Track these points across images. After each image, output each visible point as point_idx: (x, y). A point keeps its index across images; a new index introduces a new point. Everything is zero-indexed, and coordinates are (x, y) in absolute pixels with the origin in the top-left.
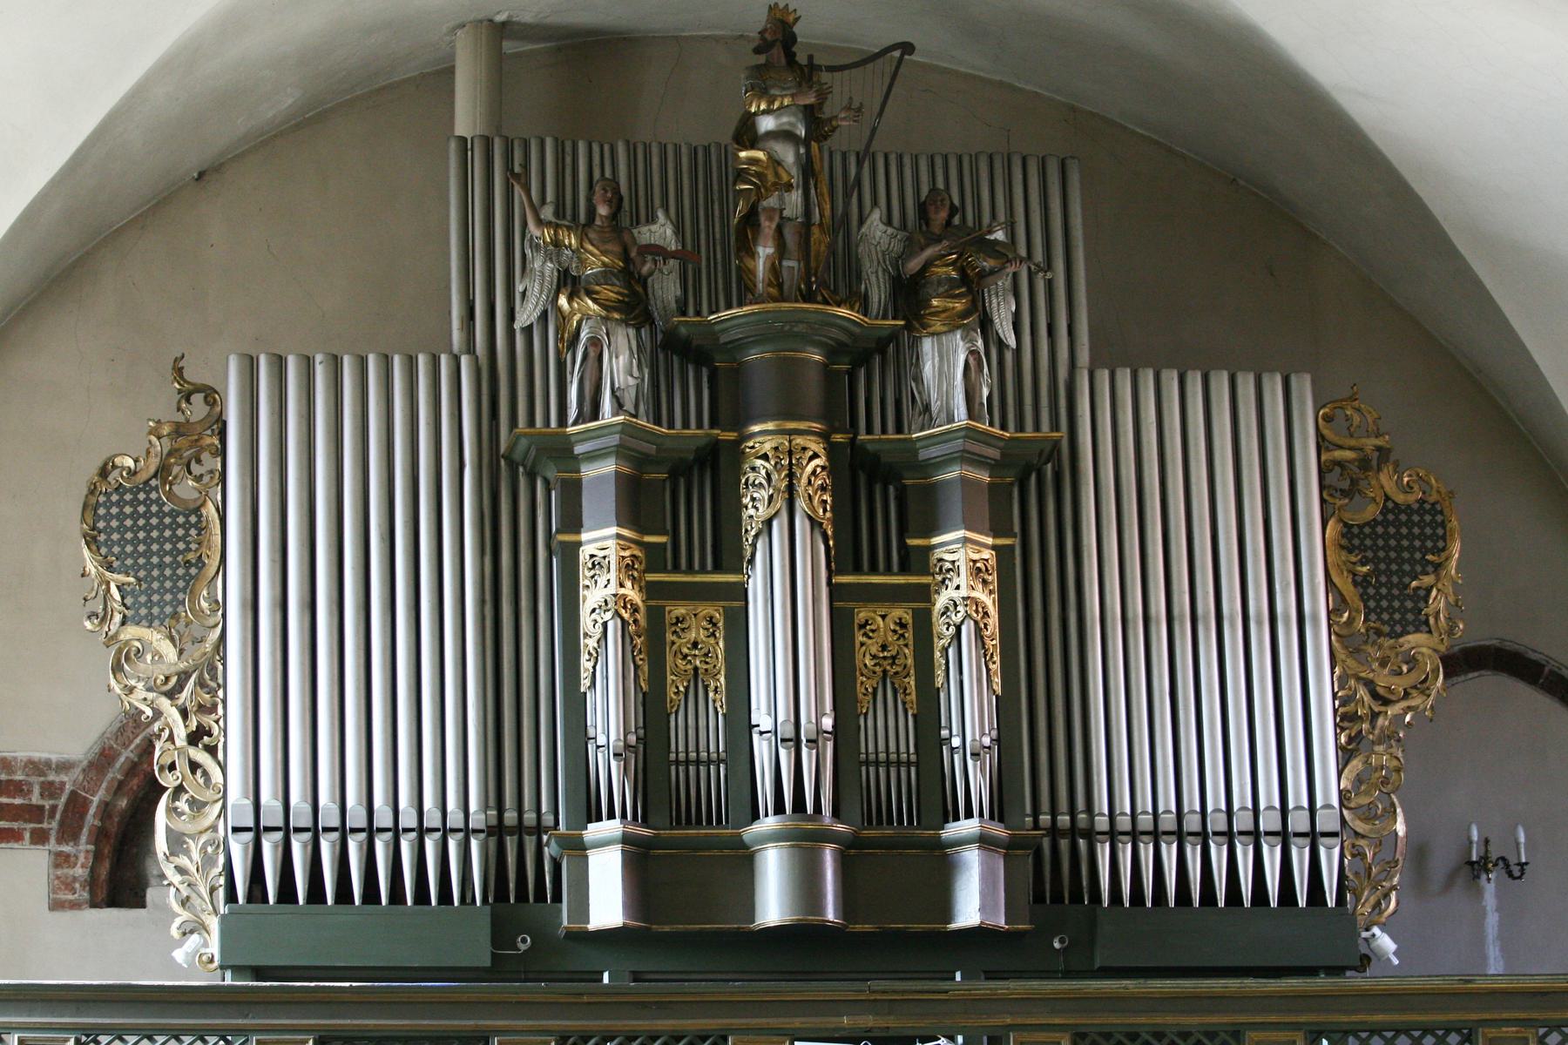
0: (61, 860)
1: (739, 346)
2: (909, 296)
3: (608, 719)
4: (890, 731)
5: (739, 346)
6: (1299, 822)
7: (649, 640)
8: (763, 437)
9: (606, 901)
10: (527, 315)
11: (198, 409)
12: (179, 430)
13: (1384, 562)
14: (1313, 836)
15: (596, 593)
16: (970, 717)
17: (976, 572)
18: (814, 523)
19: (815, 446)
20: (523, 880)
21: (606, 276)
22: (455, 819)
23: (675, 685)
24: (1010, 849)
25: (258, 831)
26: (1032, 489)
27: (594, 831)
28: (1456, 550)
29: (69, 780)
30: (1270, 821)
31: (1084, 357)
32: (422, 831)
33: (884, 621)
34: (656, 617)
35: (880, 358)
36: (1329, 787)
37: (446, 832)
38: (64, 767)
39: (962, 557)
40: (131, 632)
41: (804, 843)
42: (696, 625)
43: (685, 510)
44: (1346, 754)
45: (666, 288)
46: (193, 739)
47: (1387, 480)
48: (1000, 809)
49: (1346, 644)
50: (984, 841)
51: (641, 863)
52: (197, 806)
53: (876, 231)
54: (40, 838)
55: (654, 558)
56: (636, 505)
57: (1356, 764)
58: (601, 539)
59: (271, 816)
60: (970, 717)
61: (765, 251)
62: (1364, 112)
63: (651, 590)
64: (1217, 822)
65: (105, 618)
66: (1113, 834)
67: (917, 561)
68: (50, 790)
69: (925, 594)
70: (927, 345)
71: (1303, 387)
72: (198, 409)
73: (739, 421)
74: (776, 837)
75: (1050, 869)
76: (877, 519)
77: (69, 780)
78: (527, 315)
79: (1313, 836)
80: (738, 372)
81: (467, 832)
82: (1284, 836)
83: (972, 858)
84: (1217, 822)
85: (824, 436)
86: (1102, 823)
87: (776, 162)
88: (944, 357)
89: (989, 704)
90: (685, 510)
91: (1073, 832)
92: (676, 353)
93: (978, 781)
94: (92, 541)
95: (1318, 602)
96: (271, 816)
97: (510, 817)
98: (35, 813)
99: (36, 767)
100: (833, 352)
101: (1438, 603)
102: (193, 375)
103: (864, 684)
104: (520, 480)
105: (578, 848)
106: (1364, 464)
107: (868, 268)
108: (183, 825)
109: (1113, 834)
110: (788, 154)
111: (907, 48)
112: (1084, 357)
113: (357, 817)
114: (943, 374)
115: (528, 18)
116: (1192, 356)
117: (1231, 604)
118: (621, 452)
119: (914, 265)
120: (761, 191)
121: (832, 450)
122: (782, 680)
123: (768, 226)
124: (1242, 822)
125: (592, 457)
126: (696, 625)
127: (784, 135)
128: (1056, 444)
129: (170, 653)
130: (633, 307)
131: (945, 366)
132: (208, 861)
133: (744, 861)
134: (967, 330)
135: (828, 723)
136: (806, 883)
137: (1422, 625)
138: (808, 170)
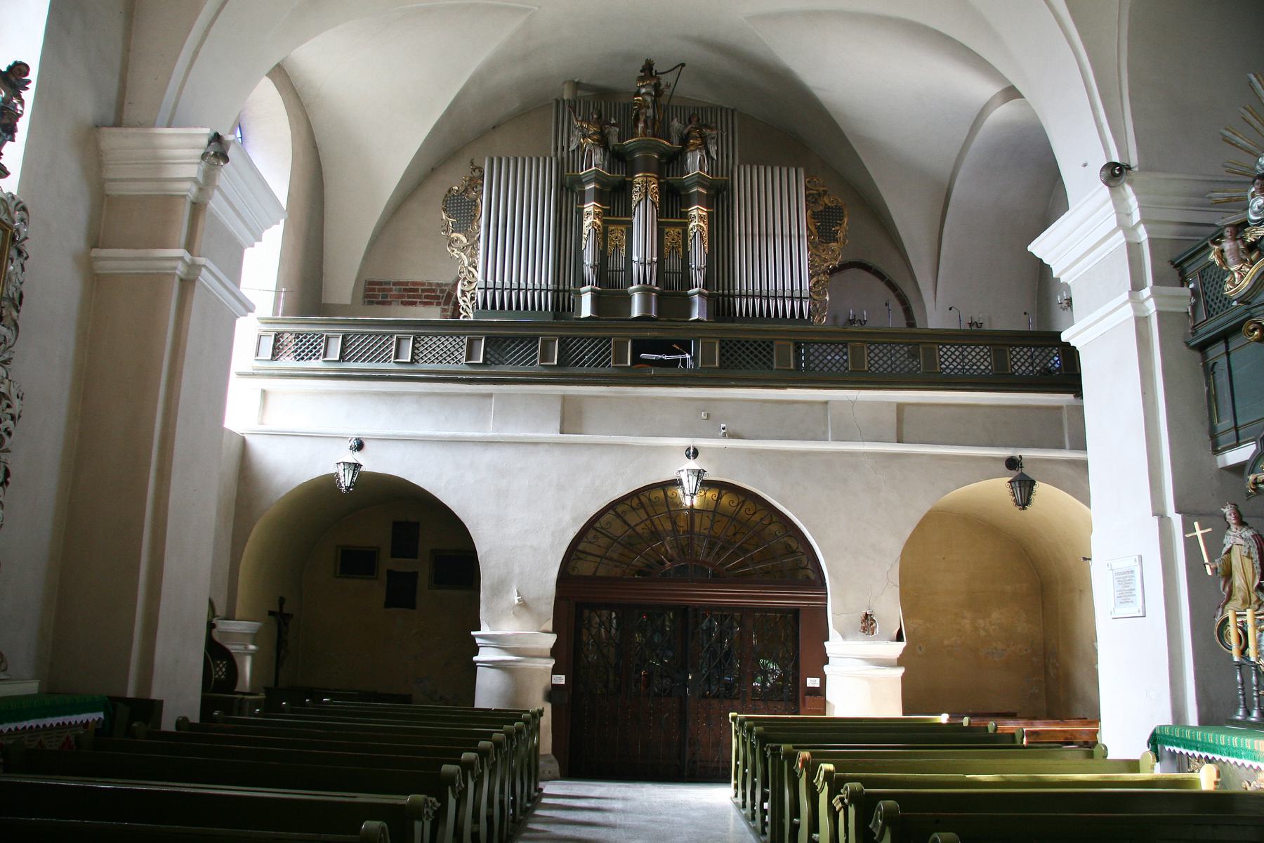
0: (444, 310)
1: (632, 153)
2: (684, 140)
3: (589, 258)
4: (674, 264)
5: (632, 153)
6: (797, 294)
7: (603, 235)
8: (639, 178)
9: (586, 311)
10: (573, 147)
11: (477, 173)
12: (471, 179)
13: (824, 225)
14: (801, 298)
15: (587, 222)
16: (698, 258)
17: (701, 217)
18: (653, 203)
19: (654, 180)
20: (563, 304)
21: (595, 133)
22: (544, 287)
23: (610, 249)
24: (709, 297)
25: (486, 289)
26: (719, 197)
27: (583, 289)
28: (846, 220)
29: (447, 289)
30: (788, 293)
31: (737, 162)
32: (534, 290)
33: (673, 232)
34: (605, 229)
35: (674, 160)
36: (806, 285)
37: (541, 290)
38: (447, 285)
39: (697, 212)
40: (454, 235)
41: (646, 291)
42: (617, 233)
43: (615, 199)
44: (811, 277)
45: (614, 140)
46: (470, 265)
47: (826, 200)
48: (705, 286)
49: (811, 244)
50: (700, 293)
51: (597, 300)
52: (470, 283)
53: (676, 124)
54: (438, 304)
55: (606, 213)
56: (599, 196)
57: (815, 279)
58: (589, 207)
59: (490, 284)
60: (698, 258)
61: (641, 125)
62: (820, 94)
63: (604, 222)
64: (772, 293)
65: (447, 231)
66: (740, 296)
67: (685, 215)
68: (442, 291)
69: (686, 225)
70: (689, 154)
71: (802, 171)
72: (477, 173)
73: (632, 175)
74: (637, 290)
75: (721, 307)
76: (672, 203)
77: (447, 289)
78: (573, 147)
79: (801, 298)
80: (633, 160)
81: (548, 290)
82: (792, 298)
83: (696, 298)
84: (772, 293)
85: (658, 179)
86: (737, 292)
87: (644, 100)
88: (694, 158)
89: (704, 257)
90: (615, 199)
91: (729, 295)
92: (618, 158)
93: (699, 278)
94: (445, 210)
95: (804, 232)
96: (490, 284)
97: (561, 287)
98: (438, 297)
99: (438, 285)
100: (661, 155)
101: (840, 234)
102: (477, 164)
103: (666, 250)
104: (568, 192)
105: (579, 294)
106: (819, 195)
107: (673, 134)
108: (466, 288)
109: (740, 296)
110: (649, 99)
111: (683, 65)
112: (737, 162)
113: (515, 285)
114: (693, 162)
115: (584, 81)
116: (769, 162)
117: (778, 231)
118: (596, 180)
119: (686, 131)
120: (640, 108)
121: (659, 184)
122: (641, 247)
123: (642, 118)
124: (780, 293)
125: (588, 182)
126: (617, 233)
127: (648, 93)
128: (727, 181)
129: (464, 240)
130: (603, 142)
131: (694, 162)
132: (472, 299)
133: (628, 299)
134: (700, 150)
135: (655, 259)
136: (646, 304)
137: (836, 240)
138: (654, 102)
